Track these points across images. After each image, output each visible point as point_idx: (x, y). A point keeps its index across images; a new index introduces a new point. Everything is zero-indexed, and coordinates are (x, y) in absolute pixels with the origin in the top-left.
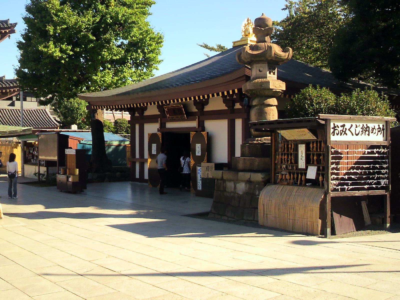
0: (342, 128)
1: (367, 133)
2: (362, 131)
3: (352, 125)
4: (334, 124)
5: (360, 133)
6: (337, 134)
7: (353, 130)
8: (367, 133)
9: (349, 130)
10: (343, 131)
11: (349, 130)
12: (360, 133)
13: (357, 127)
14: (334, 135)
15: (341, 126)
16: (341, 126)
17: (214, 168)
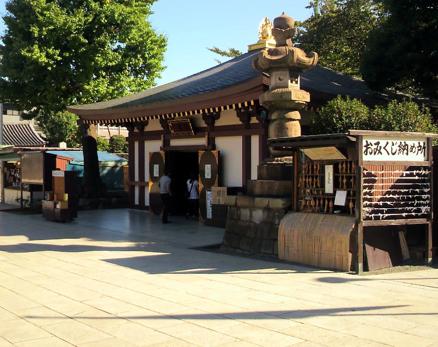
0: (376, 147)
1: (405, 151)
2: (400, 150)
3: (387, 143)
4: (367, 142)
5: (397, 152)
6: (371, 153)
7: (388, 148)
8: (405, 151)
9: (384, 148)
10: (377, 149)
11: (384, 148)
12: (397, 152)
13: (393, 145)
14: (366, 154)
15: (375, 144)
16: (375, 144)
17: (226, 193)
